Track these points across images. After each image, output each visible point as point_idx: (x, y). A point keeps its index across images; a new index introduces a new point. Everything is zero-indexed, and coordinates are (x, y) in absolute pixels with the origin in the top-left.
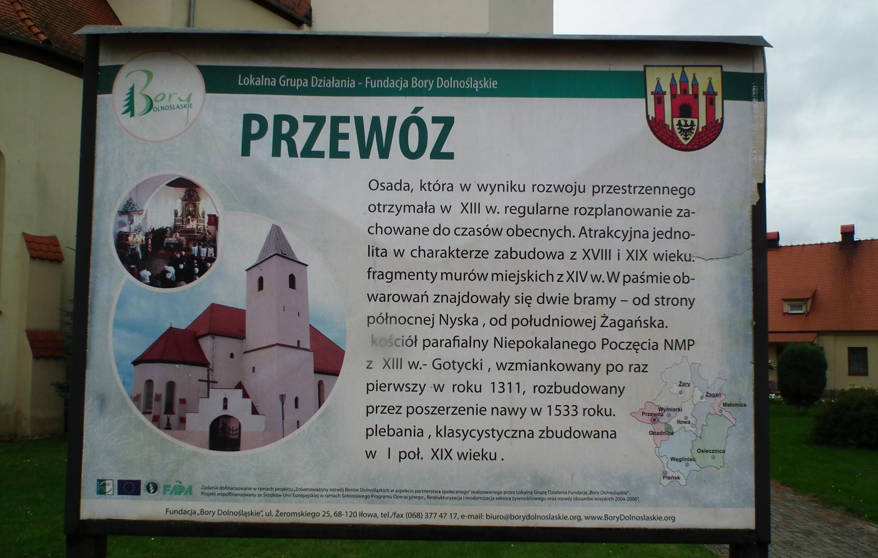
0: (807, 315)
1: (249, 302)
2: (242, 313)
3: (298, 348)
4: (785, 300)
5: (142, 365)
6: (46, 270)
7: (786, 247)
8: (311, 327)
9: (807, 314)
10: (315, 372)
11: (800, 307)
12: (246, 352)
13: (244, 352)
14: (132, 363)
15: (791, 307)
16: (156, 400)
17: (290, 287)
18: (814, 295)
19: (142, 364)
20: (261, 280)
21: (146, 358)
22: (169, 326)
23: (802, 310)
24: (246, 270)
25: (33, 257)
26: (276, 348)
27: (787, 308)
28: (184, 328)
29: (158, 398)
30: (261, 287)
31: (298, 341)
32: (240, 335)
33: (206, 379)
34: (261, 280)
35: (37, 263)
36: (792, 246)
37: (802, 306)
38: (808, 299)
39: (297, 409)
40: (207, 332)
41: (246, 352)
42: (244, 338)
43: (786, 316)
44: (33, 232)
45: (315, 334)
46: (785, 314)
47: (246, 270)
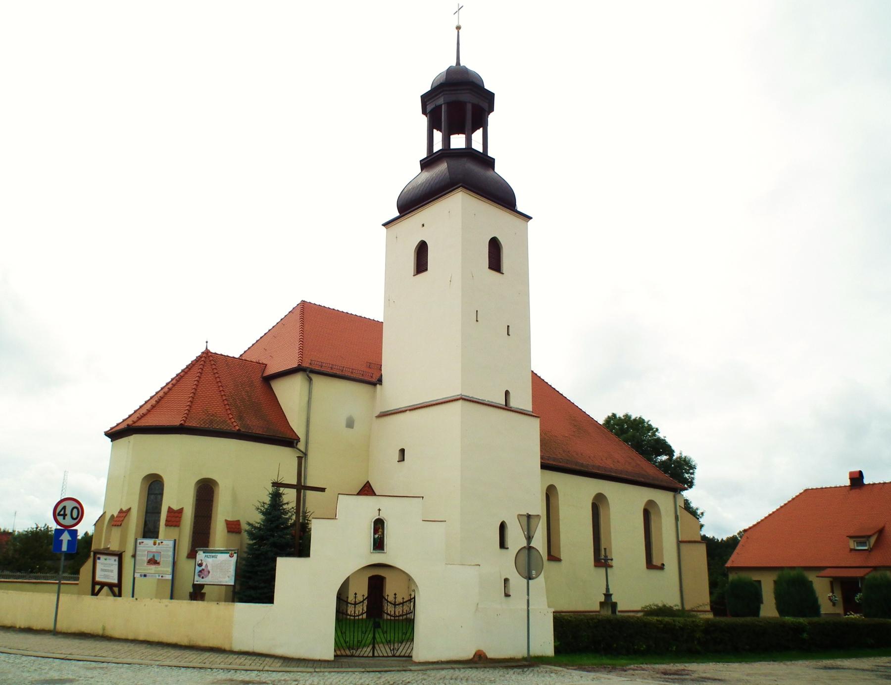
0: (870, 551)
1: (389, 302)
2: (375, 328)
3: (507, 407)
4: (851, 537)
5: (134, 439)
6: (235, 537)
7: (869, 484)
8: (534, 375)
9: (869, 551)
10: (544, 466)
11: (864, 544)
12: (384, 415)
13: (377, 413)
14: (108, 434)
15: (857, 543)
16: (169, 523)
17: (490, 268)
18: (881, 532)
19: (134, 436)
20: (422, 250)
21: (144, 423)
22: (203, 349)
23: (866, 546)
24: (384, 225)
25: (229, 532)
26: (460, 402)
27: (852, 544)
28: (237, 356)
29: (175, 517)
30: (421, 265)
31: (507, 393)
32: (373, 378)
33: (295, 482)
34: (422, 250)
35: (230, 534)
36: (874, 484)
37: (866, 543)
38: (869, 537)
39: (504, 551)
40: (295, 365)
41: (384, 415)
42: (380, 381)
43: (853, 551)
44: (229, 519)
45: (539, 385)
46: (851, 550)
47: (384, 225)
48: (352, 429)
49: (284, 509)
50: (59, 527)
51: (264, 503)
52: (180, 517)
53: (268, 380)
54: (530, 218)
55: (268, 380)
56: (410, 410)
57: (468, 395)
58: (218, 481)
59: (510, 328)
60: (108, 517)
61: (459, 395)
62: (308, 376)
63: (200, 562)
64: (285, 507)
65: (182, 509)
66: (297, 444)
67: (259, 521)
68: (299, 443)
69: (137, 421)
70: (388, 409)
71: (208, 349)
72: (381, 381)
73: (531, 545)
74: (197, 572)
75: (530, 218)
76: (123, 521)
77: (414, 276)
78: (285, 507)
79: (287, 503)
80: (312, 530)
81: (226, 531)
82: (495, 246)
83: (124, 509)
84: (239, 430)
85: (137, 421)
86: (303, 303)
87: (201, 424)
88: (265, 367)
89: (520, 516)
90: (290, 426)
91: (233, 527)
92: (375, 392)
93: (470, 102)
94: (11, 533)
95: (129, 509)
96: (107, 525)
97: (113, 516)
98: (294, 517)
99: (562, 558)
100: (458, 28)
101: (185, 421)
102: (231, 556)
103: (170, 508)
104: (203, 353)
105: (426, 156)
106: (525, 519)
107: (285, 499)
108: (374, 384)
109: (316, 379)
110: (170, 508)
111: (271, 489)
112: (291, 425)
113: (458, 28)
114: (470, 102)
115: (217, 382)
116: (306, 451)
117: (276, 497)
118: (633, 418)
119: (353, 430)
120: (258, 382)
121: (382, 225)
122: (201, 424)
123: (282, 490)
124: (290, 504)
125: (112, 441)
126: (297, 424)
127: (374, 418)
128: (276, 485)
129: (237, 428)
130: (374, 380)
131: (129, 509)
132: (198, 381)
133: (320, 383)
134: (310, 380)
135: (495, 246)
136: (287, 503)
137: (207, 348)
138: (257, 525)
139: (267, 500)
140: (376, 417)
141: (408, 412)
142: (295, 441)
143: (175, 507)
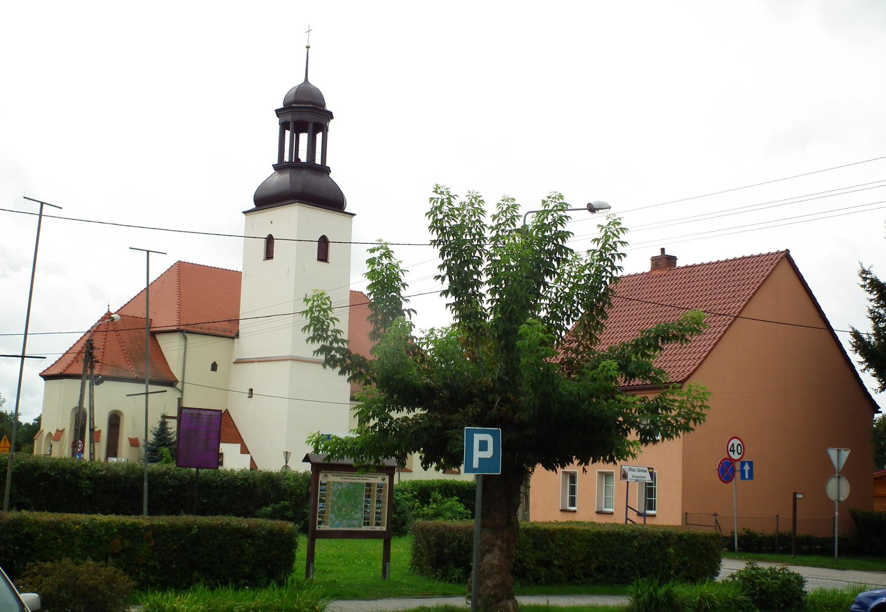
2: (239, 274)
22: (106, 311)
24: (245, 213)
25: (131, 445)
35: (132, 447)
42: (237, 336)
44: (131, 437)
49: (169, 432)
51: (155, 428)
52: (100, 436)
53: (153, 334)
54: (354, 215)
55: (153, 334)
56: (258, 362)
57: (295, 355)
58: (124, 412)
61: (289, 356)
62: (184, 336)
64: (169, 430)
66: (176, 385)
67: (152, 440)
68: (177, 384)
69: (66, 369)
70: (243, 358)
71: (110, 311)
72: (238, 336)
73: (288, 464)
75: (354, 215)
76: (60, 437)
77: (264, 260)
78: (169, 430)
79: (171, 428)
81: (129, 445)
82: (324, 243)
83: (60, 429)
84: (137, 377)
85: (66, 369)
86: (179, 262)
87: (111, 373)
88: (151, 321)
89: (284, 452)
90: (170, 370)
91: (134, 443)
92: (233, 346)
93: (311, 122)
95: (64, 430)
96: (46, 439)
97: (50, 434)
98: (175, 438)
100: (308, 47)
101: (100, 372)
104: (106, 314)
106: (285, 454)
107: (169, 425)
108: (233, 338)
109: (189, 336)
111: (160, 419)
112: (171, 369)
113: (308, 47)
114: (311, 122)
115: (121, 346)
116: (184, 336)
117: (163, 424)
120: (145, 333)
121: (243, 212)
122: (111, 373)
123: (167, 420)
124: (173, 429)
125: (44, 380)
126: (175, 369)
127: (232, 363)
128: (164, 417)
129: (136, 376)
130: (233, 335)
131: (64, 430)
132: (105, 339)
133: (192, 339)
134: (186, 338)
135: (324, 243)
136: (171, 428)
137: (109, 310)
138: (150, 442)
139: (158, 426)
140: (234, 363)
141: (256, 363)
142: (175, 383)
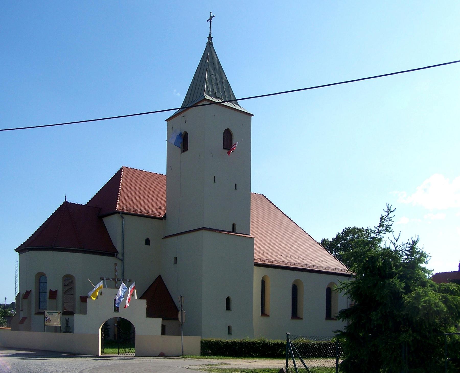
12: (166, 237)
29: (53, 295)
48: (149, 246)
50: (284, 369)
59: (237, 186)
60: (21, 295)
63: (46, 316)
65: (57, 290)
68: (118, 255)
74: (45, 320)
80: (290, 317)
83: (29, 290)
94: (346, 332)
99: (232, 333)
102: (59, 314)
103: (51, 291)
105: (180, 107)
110: (51, 291)
118: (331, 239)
119: (50, 289)
143: (53, 290)
